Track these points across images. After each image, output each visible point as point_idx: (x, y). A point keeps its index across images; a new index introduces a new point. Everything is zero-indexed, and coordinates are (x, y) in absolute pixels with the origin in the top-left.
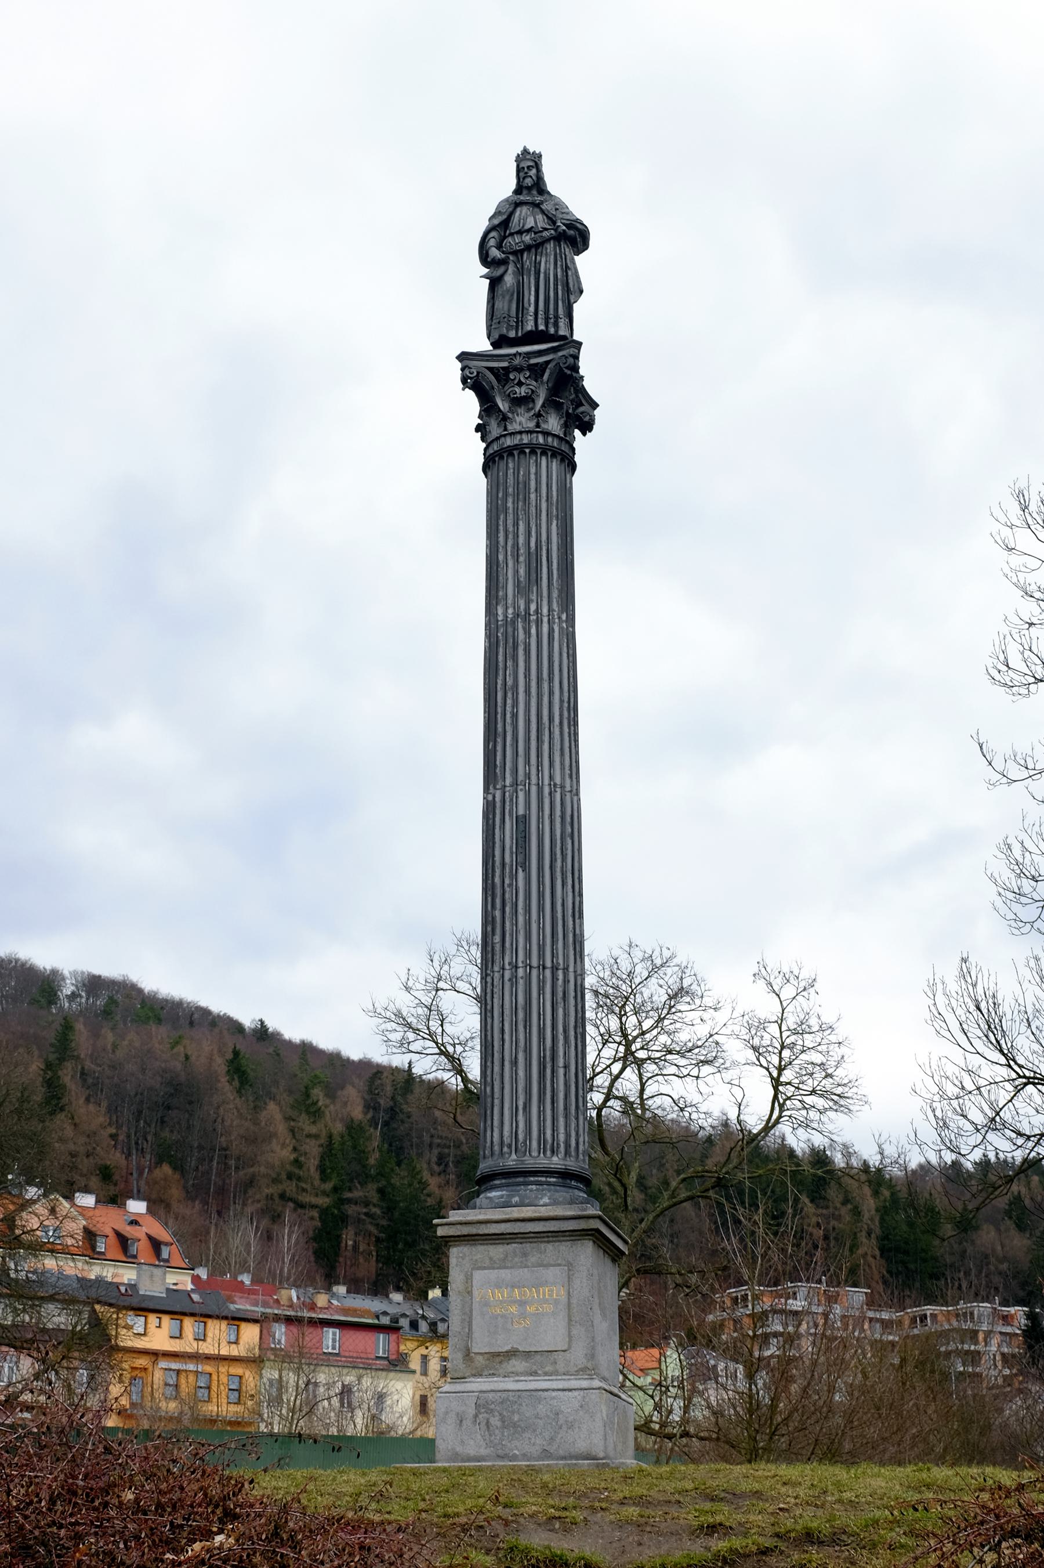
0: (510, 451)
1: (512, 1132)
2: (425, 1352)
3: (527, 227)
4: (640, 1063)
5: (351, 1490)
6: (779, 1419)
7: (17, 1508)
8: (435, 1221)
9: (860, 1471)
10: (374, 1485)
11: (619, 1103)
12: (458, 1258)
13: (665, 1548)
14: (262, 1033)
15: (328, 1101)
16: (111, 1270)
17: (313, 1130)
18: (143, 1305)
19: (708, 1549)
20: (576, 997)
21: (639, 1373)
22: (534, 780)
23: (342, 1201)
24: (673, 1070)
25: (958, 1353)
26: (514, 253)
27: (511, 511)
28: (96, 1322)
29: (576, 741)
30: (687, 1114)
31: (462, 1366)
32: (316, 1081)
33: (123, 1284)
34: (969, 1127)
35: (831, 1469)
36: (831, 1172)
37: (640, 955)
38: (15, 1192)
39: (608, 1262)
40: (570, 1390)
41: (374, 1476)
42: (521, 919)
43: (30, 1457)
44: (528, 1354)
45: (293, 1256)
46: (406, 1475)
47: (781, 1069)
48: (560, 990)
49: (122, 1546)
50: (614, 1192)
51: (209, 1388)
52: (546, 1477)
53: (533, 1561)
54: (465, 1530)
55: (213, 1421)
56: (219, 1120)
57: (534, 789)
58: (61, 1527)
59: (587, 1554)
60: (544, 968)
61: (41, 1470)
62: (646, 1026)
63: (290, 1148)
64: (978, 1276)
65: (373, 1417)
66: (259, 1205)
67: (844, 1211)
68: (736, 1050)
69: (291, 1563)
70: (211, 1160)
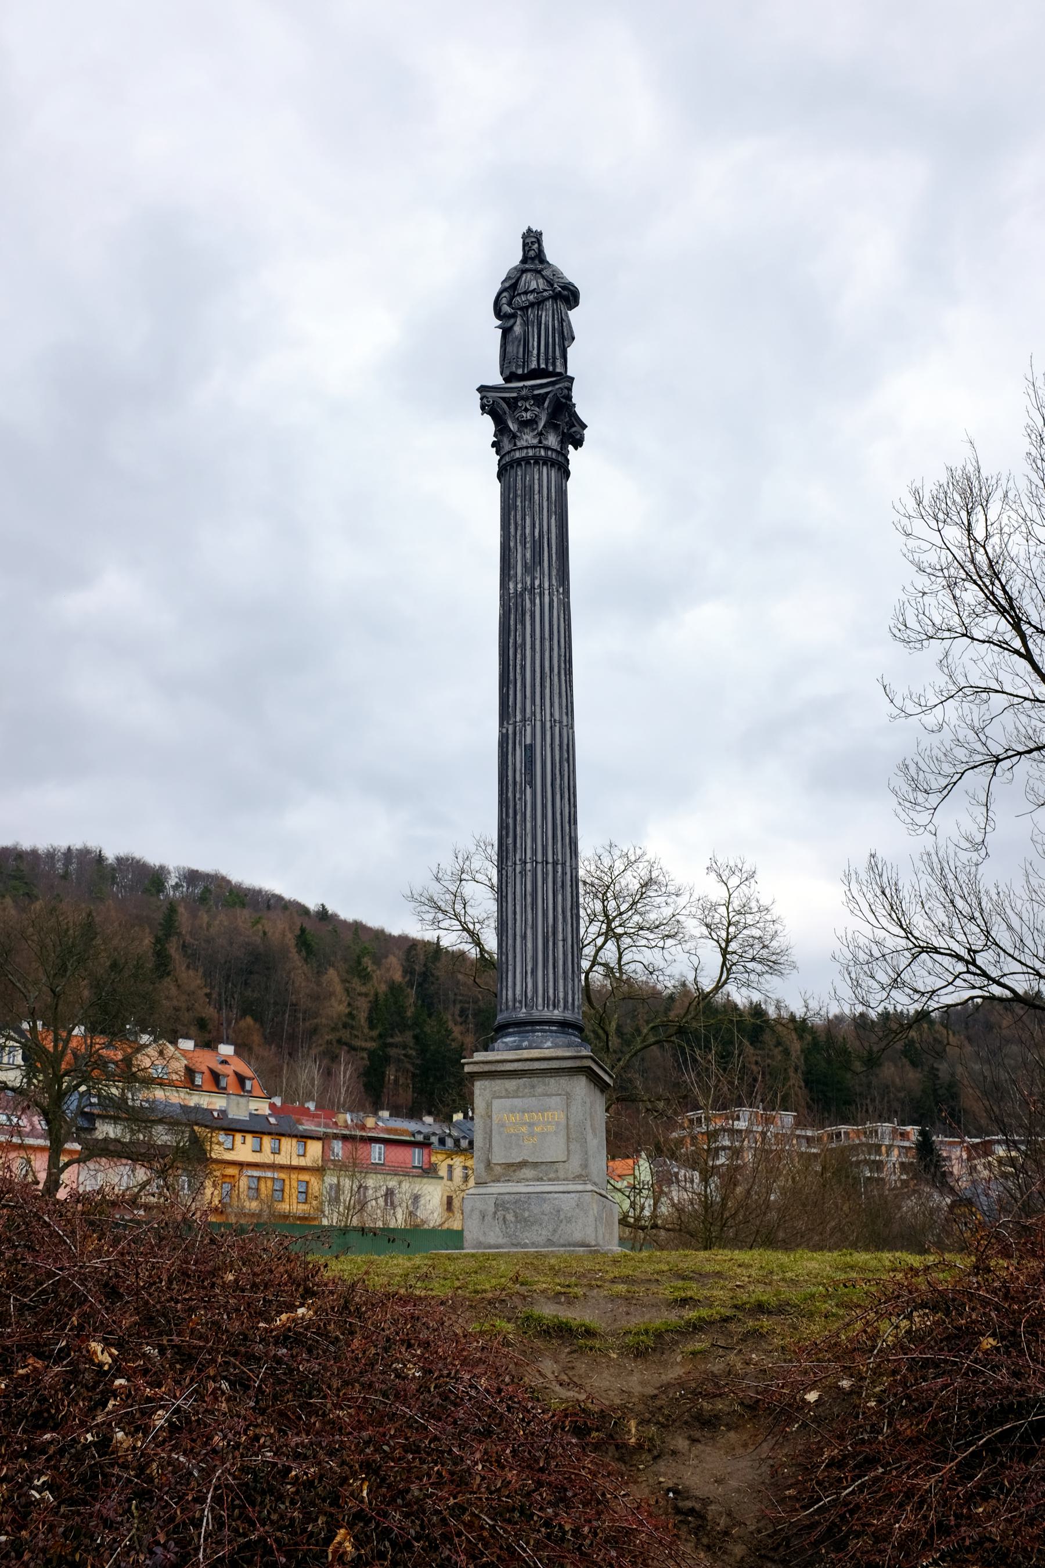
0: (518, 462)
1: (517, 990)
2: (451, 1163)
3: (531, 288)
4: (618, 937)
5: (401, 1272)
6: (727, 1214)
7: (143, 1288)
8: (463, 1061)
9: (798, 1256)
10: (419, 1267)
11: (602, 968)
12: (481, 1090)
13: (647, 1316)
14: (323, 915)
15: (375, 968)
16: (207, 1099)
17: (364, 990)
18: (232, 1126)
19: (681, 1317)
20: (572, 886)
21: (617, 1179)
22: (538, 717)
23: (386, 1045)
24: (644, 942)
25: (866, 1162)
26: (522, 309)
27: (519, 508)
28: (196, 1141)
29: (571, 686)
30: (655, 977)
31: (484, 1174)
32: (365, 952)
33: (215, 1110)
34: (876, 985)
35: (775, 1254)
36: (767, 1021)
37: (618, 853)
38: (132, 1038)
39: (598, 1093)
40: (569, 1192)
41: (417, 1261)
42: (529, 825)
43: (153, 1247)
44: (535, 1165)
45: (348, 1087)
46: (443, 1260)
47: (728, 941)
48: (559, 880)
49: (225, 1317)
50: (598, 1037)
51: (283, 1191)
52: (553, 1261)
53: (545, 1327)
54: (490, 1303)
55: (286, 1217)
56: (291, 982)
57: (538, 724)
58: (177, 1302)
59: (587, 1322)
60: (547, 863)
61: (161, 1257)
62: (623, 908)
63: (346, 1004)
64: (881, 1102)
65: (411, 1213)
66: (321, 1048)
67: (776, 1051)
68: (693, 927)
69: (358, 1329)
70: (284, 1013)
